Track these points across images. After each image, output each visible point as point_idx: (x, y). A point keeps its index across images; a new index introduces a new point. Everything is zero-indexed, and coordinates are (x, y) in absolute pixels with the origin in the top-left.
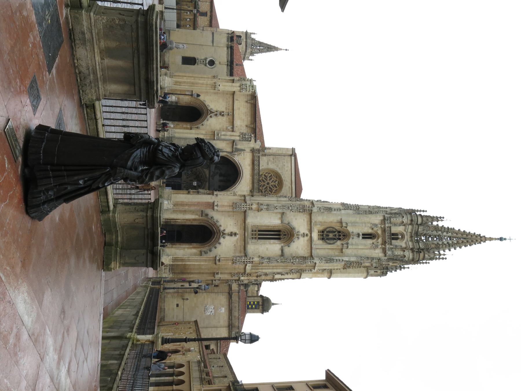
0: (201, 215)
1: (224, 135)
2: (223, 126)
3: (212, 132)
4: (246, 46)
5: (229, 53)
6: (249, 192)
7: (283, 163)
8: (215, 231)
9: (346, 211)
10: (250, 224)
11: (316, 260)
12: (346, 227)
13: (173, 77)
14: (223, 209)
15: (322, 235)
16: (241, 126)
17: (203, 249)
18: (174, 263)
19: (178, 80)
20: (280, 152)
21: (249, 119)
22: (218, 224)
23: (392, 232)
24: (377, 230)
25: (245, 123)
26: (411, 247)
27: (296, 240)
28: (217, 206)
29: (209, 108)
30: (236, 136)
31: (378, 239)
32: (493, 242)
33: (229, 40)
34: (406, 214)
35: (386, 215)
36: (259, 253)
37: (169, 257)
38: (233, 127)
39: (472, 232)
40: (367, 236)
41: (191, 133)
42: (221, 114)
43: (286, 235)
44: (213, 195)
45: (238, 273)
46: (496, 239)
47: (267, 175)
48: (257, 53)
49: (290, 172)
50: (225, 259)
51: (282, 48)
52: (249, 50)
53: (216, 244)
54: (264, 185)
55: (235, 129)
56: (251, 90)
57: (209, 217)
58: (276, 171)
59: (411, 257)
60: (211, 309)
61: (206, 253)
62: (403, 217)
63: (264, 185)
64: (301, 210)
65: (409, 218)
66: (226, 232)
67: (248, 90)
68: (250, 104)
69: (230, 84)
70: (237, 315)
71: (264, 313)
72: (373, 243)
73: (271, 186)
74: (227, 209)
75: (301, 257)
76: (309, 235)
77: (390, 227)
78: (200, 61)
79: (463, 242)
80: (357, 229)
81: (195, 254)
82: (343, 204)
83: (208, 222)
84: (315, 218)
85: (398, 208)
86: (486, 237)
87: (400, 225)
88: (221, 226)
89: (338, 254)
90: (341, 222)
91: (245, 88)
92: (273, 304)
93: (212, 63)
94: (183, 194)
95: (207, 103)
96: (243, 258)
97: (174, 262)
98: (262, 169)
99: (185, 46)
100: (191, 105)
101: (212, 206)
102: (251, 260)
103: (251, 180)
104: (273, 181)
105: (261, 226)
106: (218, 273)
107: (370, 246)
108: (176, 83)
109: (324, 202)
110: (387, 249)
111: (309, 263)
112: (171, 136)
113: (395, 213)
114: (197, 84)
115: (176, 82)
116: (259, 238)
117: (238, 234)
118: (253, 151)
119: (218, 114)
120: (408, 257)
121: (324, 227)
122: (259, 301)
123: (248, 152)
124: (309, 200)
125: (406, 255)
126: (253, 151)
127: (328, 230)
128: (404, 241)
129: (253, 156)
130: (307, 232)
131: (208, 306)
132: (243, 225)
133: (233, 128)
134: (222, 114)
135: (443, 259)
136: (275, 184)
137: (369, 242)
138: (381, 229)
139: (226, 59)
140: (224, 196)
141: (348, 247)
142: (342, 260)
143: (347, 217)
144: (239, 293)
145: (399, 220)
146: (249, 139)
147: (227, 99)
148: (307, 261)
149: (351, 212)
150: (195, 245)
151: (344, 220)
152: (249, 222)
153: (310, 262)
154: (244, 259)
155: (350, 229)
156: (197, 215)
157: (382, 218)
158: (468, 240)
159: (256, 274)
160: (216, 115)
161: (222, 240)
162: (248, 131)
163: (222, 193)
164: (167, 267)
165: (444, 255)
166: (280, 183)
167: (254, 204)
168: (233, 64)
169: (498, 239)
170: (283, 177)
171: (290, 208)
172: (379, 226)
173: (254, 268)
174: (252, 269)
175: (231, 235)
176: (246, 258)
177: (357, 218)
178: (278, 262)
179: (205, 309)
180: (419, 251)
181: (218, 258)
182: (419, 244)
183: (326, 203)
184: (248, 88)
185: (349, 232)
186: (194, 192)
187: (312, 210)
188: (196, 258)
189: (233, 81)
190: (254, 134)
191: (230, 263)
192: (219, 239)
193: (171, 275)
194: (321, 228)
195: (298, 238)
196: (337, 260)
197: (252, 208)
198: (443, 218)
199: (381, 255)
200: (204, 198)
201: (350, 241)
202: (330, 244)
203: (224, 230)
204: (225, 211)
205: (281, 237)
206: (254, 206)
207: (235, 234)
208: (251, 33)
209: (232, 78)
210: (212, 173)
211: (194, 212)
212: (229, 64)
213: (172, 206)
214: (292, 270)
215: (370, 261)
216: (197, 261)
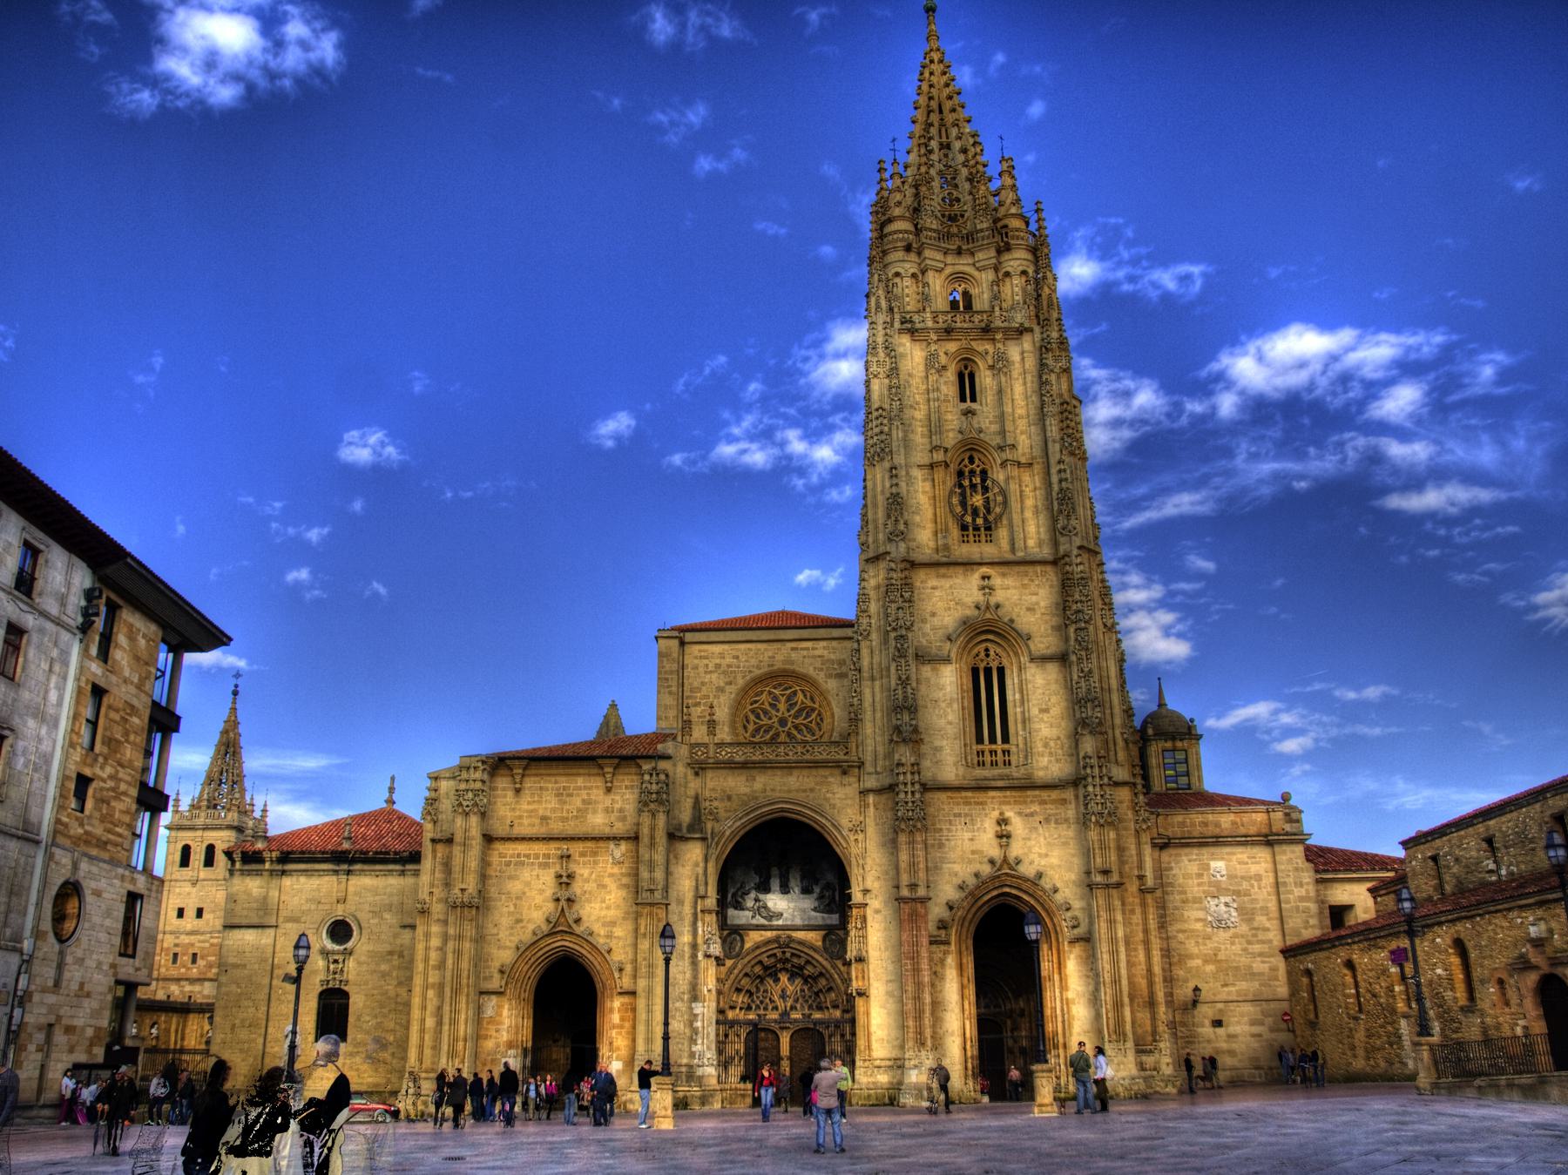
0: (942, 947)
2: (611, 875)
6: (846, 779)
7: (711, 672)
8: (995, 893)
10: (961, 770)
12: (946, 450)
16: (607, 811)
18: (1130, 1035)
22: (971, 881)
24: (946, 354)
26: (993, 253)
30: (653, 829)
34: (885, 266)
36: (1059, 738)
38: (615, 838)
43: (987, 650)
45: (1134, 808)
47: (751, 727)
57: (945, 914)
58: (737, 694)
62: (897, 274)
64: (907, 595)
67: (478, 785)
68: (527, 779)
71: (1199, 732)
72: (992, 367)
73: (792, 712)
76: (984, 570)
78: (335, 973)
80: (949, 417)
83: (964, 918)
87: (926, 285)
88: (977, 875)
91: (470, 795)
94: (868, 1014)
95: (527, 937)
97: (1125, 1035)
100: (532, 997)
102: (1094, 761)
104: (773, 706)
116: (1006, 739)
117: (1002, 814)
120: (1025, 263)
125: (1021, 268)
127: (959, 509)
128: (976, 273)
130: (975, 579)
131: (1210, 918)
132: (969, 794)
134: (565, 880)
136: (783, 699)
137: (985, 379)
138: (943, 343)
139: (327, 878)
142: (1059, 462)
146: (662, 777)
147: (508, 864)
152: (957, 775)
155: (951, 439)
156: (942, 961)
161: (1027, 870)
162: (626, 787)
166: (781, 677)
175: (1008, 836)
184: (472, 785)
194: (955, 532)
195: (998, 606)
196: (1061, 481)
197: (913, 765)
199: (1027, 343)
203: (992, 862)
205: (994, 665)
207: (1002, 821)
210: (760, 921)
211: (935, 973)
212: (345, 867)
215: (1053, 377)
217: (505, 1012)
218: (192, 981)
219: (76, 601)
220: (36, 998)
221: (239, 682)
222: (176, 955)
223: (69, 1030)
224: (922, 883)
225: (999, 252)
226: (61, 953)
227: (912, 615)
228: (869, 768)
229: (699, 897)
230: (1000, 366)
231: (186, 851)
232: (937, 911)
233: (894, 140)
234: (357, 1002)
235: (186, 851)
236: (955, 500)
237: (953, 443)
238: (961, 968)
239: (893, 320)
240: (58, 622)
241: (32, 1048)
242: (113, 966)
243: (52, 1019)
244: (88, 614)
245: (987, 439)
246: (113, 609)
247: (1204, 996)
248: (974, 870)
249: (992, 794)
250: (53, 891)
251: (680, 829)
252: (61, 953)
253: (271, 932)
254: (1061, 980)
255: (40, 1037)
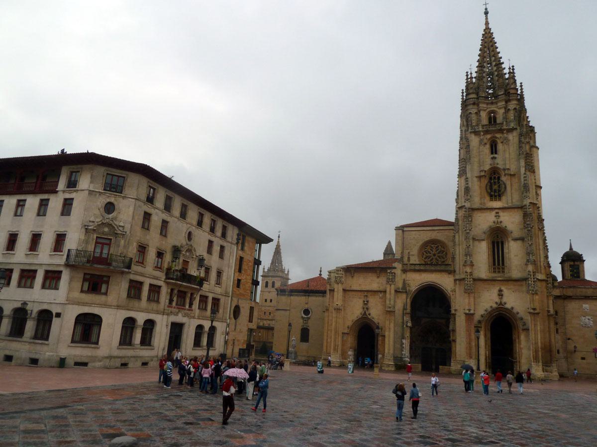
1: (390, 301)
3: (387, 314)
4: (277, 276)
5: (296, 294)
6: (450, 276)
9: (467, 172)
11: (527, 202)
12: (485, 171)
13: (328, 352)
14: (472, 303)
15: (496, 196)
16: (378, 283)
17: (521, 327)
19: (332, 347)
20: (400, 242)
21: (370, 274)
22: (489, 309)
23: (488, 123)
25: (375, 278)
26: (504, 103)
27: (503, 225)
28: (469, 310)
29: (360, 316)
30: (390, 289)
31: (496, 138)
32: (489, 20)
33: (284, 293)
35: (470, 130)
37: (533, 366)
38: (380, 291)
39: (480, 42)
40: (494, 149)
41: (389, 336)
42: (366, 304)
43: (498, 236)
44: (455, 314)
46: (487, 18)
47: (424, 256)
48: (282, 265)
49: (422, 232)
50: (85, 304)
51: (277, 241)
52: (280, 274)
53: (514, 313)
54: (436, 259)
55: (381, 289)
56: (341, 272)
59: (515, 102)
60: (586, 320)
61: (524, 324)
62: (470, 113)
63: (436, 259)
65: (471, 106)
66: (497, 300)
67: (341, 275)
69: (335, 293)
70: (592, 290)
72: (502, 142)
74: (472, 299)
75: (524, 218)
76: (497, 211)
77: (483, 126)
79: (493, 51)
80: (487, 160)
81: (527, 336)
82: (460, 176)
84: (476, 206)
85: (461, 119)
86: (485, 28)
87: (480, 116)
88: (491, 307)
89: (516, 179)
90: (480, 177)
91: (339, 278)
92: (571, 249)
93: (307, 312)
96: (530, 282)
98: (419, 261)
99: (293, 338)
101: (469, 316)
102: (532, 273)
103: (438, 273)
105: (489, 262)
106: (549, 311)
107: (506, 146)
108: (335, 350)
109: (458, 196)
110: (507, 127)
111: (531, 210)
112: (393, 358)
113: (467, 121)
114: (336, 328)
115: (335, 349)
117: (500, 288)
118: (404, 271)
119: (366, 306)
120: (515, 105)
121: (486, 196)
122: (569, 265)
123: (406, 276)
124: (457, 211)
125: (514, 107)
126: (404, 271)
127: (489, 191)
129: (411, 270)
130: (494, 213)
131: (582, 323)
133: (381, 292)
134: (366, 303)
135: (513, 69)
136: (434, 248)
137: (500, 147)
139: (302, 297)
140: (456, 303)
141: (508, 169)
143: (473, 172)
144: (563, 288)
145: (474, 118)
146: (394, 274)
148: (528, 212)
149: (468, 168)
150: (515, 336)
151: (476, 173)
153: (529, 209)
154: (531, 281)
155: (487, 167)
157: (473, 136)
158: (490, 46)
159: (547, 268)
160: (367, 309)
161: (508, 306)
163: (453, 304)
164: (545, 368)
165: (510, 68)
166: (432, 242)
167: (465, 270)
168: (308, 290)
169: (486, 16)
170: (426, 240)
171: (468, 231)
172: (482, 137)
173: (539, 270)
174: (541, 273)
175: (502, 295)
176: (530, 279)
177: (475, 160)
178: (532, 244)
179: (586, 326)
180: (507, 93)
181: (532, 311)
182: (500, 95)
183: (460, 193)
184: (339, 275)
185: (491, 169)
186: (454, 335)
187: (469, 208)
188: (533, 336)
189: (332, 291)
190: (387, 269)
191: (537, 297)
192: (507, 309)
193: (554, 365)
194: (488, 198)
195: (501, 222)
196: (525, 180)
198: (467, 72)
199: (515, 133)
200: (460, 325)
201: (500, 166)
202: (505, 188)
203: (496, 303)
204: (474, 302)
205: (500, 240)
206: (468, 270)
207: (500, 291)
208: (264, 272)
209: (328, 292)
212: (307, 294)
213: (471, 360)
214: (539, 228)
215: (523, 145)
216: (536, 334)
217: (349, 339)
218: (269, 320)
219: (235, 237)
220: (230, 333)
221: (280, 234)
222: (265, 312)
223: (238, 340)
224: (472, 308)
225: (506, 102)
226: (236, 323)
227: (471, 226)
228: (457, 272)
229: (405, 309)
230: (506, 141)
231: (267, 283)
232: (477, 317)
233: (471, 65)
234: (311, 332)
235: (267, 283)
236: (488, 187)
237: (488, 168)
238: (485, 336)
239: (468, 129)
240: (231, 243)
241: (230, 345)
242: (247, 325)
243: (234, 338)
244: (238, 239)
245: (500, 167)
246: (244, 237)
247: (579, 348)
248: (491, 305)
249: (497, 282)
250: (233, 308)
251: (399, 289)
252: (236, 323)
253: (288, 311)
254: (519, 341)
255: (232, 343)
